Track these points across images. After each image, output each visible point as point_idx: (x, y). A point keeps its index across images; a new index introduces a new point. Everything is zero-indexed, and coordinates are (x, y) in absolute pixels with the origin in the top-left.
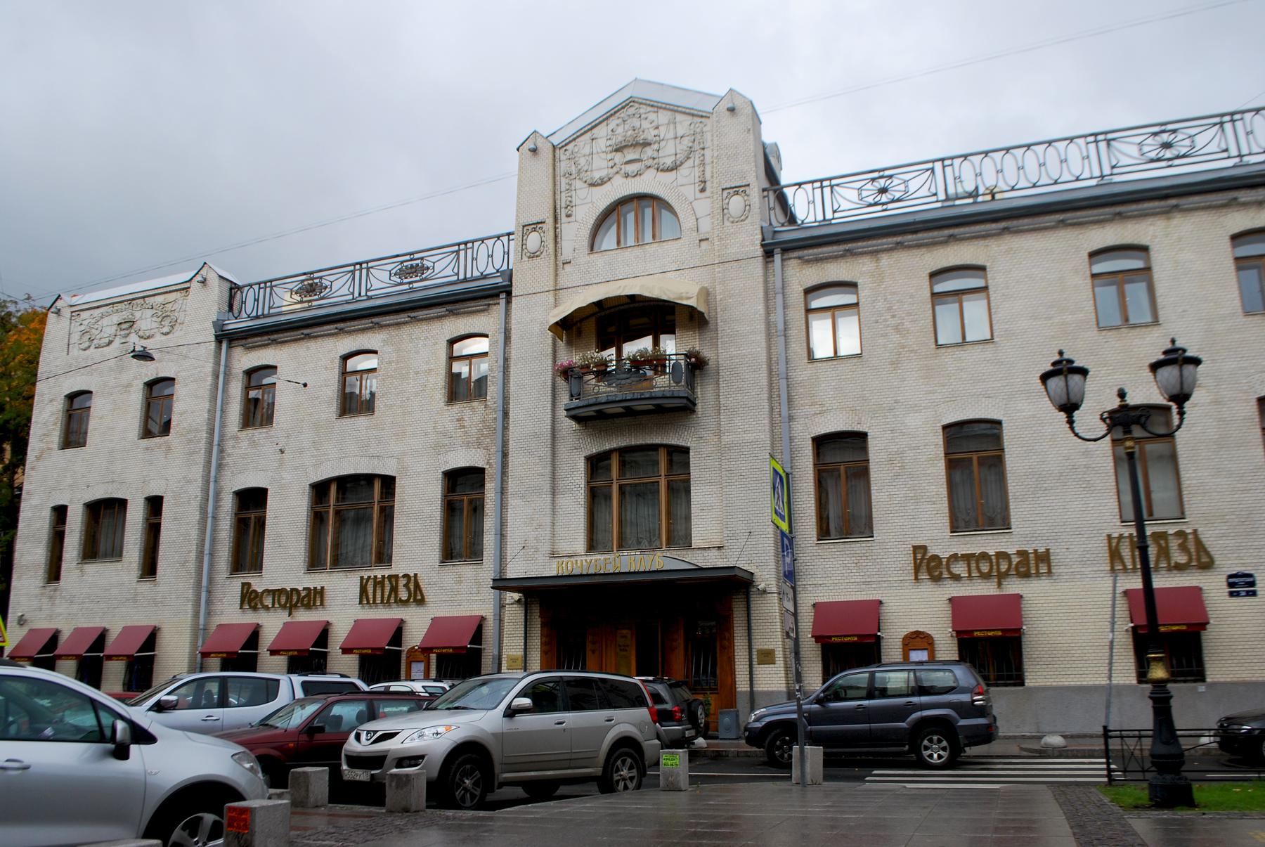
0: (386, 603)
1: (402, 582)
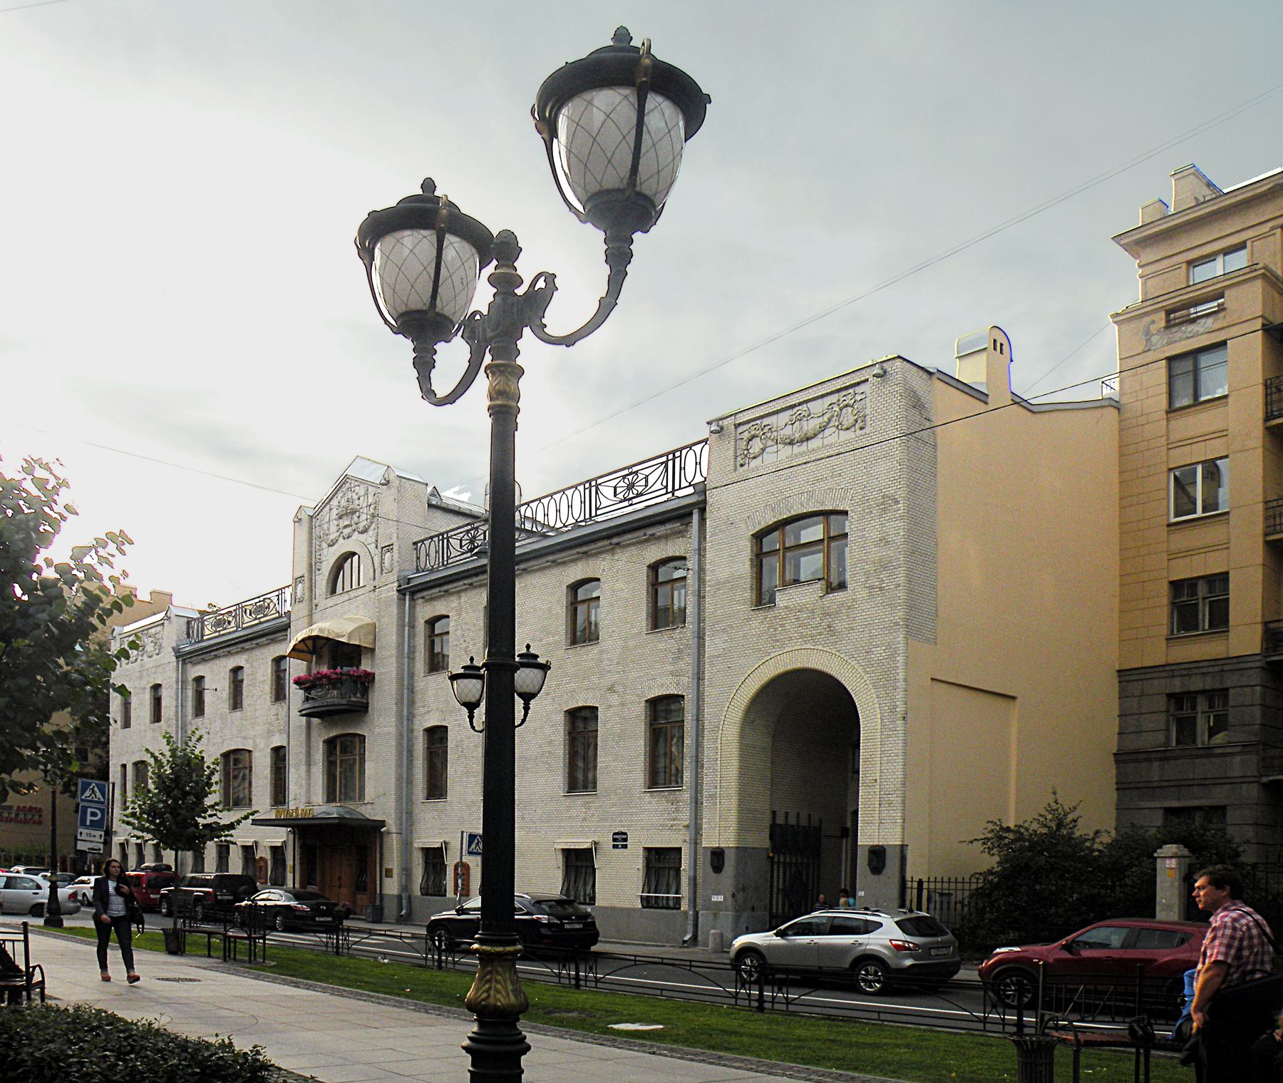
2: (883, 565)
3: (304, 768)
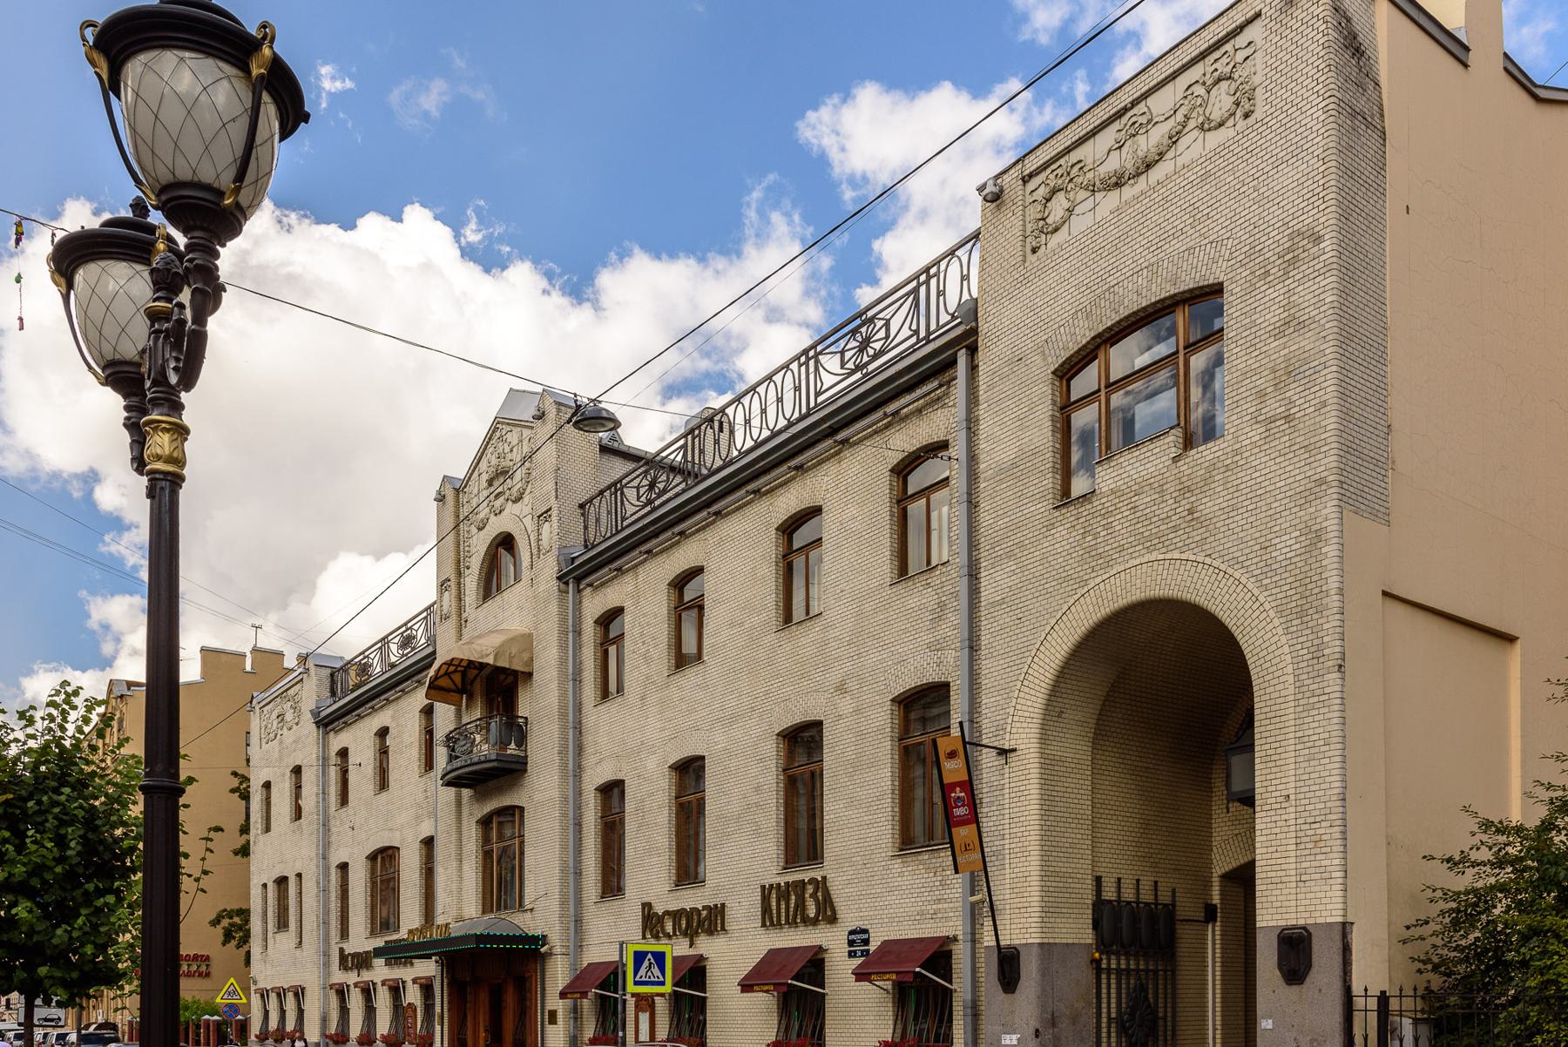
0: (792, 923)
1: (810, 889)
2: (1288, 373)
3: (455, 864)
